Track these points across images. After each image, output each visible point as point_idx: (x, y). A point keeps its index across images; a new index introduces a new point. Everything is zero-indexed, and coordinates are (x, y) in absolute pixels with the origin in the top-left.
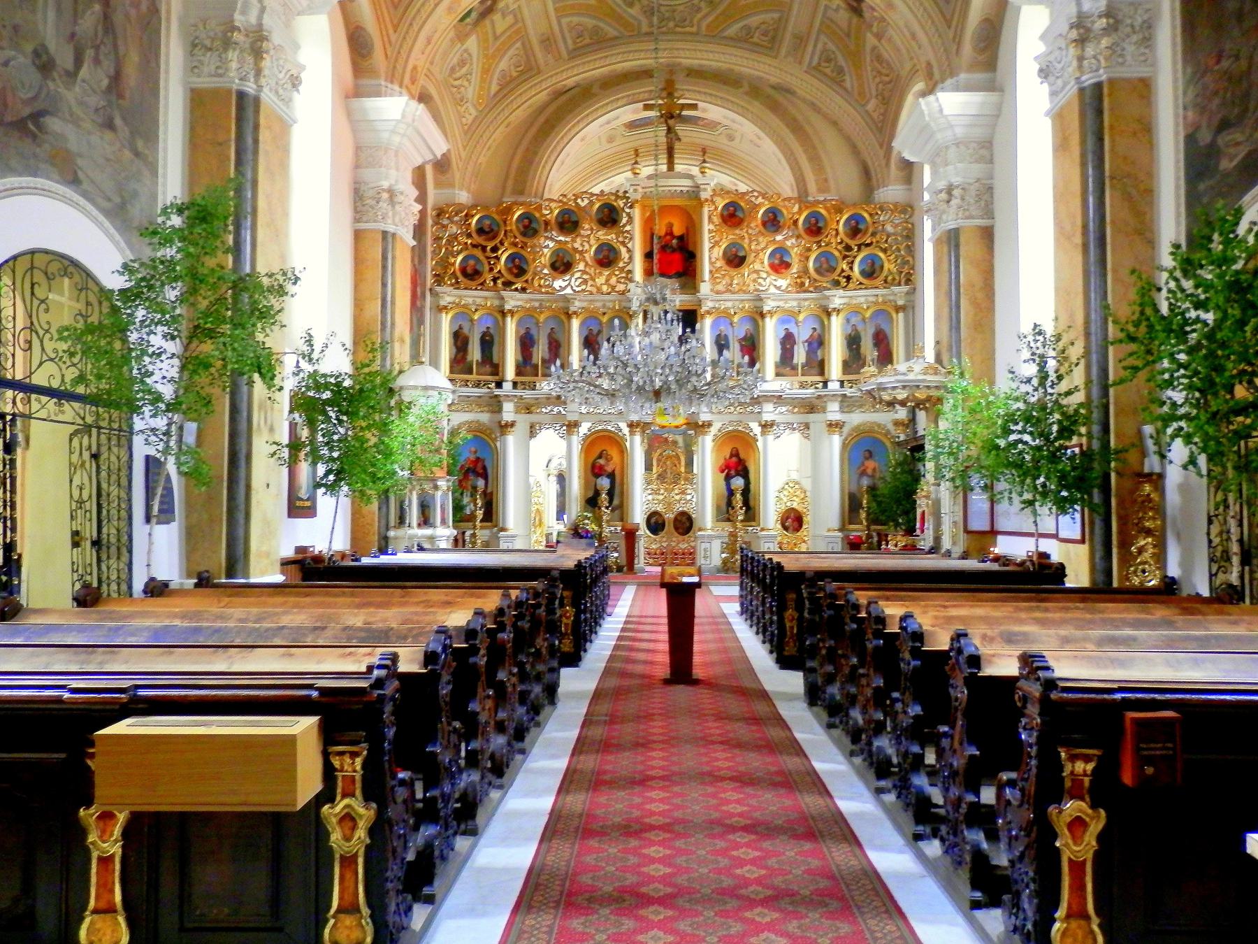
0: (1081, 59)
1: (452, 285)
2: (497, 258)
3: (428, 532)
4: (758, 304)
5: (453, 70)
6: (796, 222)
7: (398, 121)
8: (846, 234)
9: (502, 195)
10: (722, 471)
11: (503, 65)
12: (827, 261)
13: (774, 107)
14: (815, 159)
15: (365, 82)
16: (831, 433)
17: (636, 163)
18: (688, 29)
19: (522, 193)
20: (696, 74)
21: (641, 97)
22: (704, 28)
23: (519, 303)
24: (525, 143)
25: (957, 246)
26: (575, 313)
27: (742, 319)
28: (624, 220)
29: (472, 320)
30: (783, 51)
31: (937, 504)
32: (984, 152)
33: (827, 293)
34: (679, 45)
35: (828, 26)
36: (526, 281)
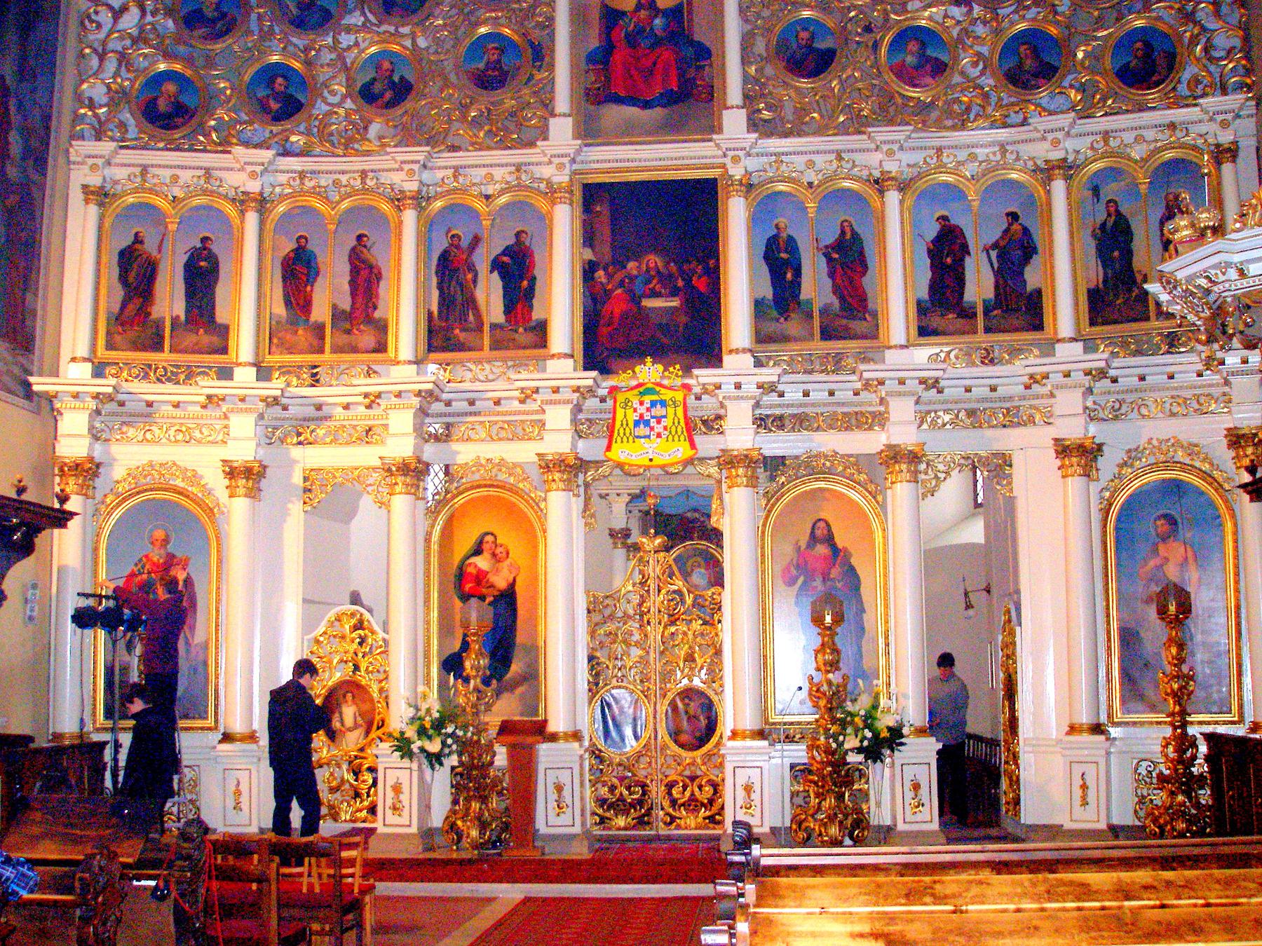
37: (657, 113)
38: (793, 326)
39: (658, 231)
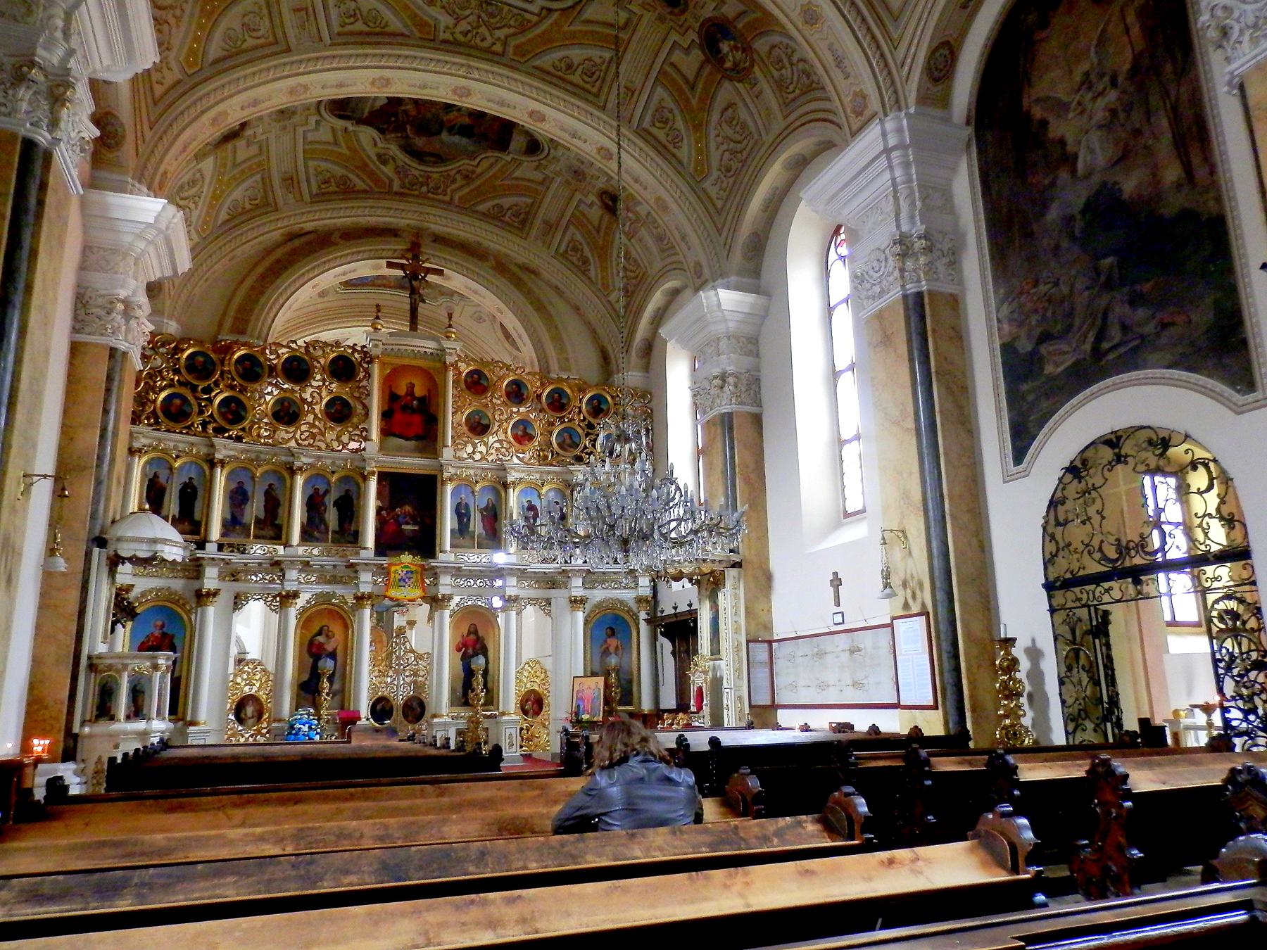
0: (902, 270)
1: (150, 425)
2: (210, 401)
3: (140, 725)
4: (501, 474)
5: (182, 187)
6: (539, 397)
7: (148, 225)
8: (588, 412)
9: (218, 332)
10: (459, 650)
11: (238, 194)
12: (571, 437)
13: (518, 283)
14: (557, 339)
15: (103, 174)
16: (573, 609)
17: (378, 318)
18: (441, 197)
19: (243, 332)
20: (439, 240)
21: (384, 254)
22: (456, 198)
23: (232, 453)
24: (249, 282)
25: (731, 429)
26: (300, 469)
27: (483, 489)
28: (362, 375)
29: (171, 469)
30: (534, 232)
31: (717, 683)
32: (750, 347)
33: (571, 468)
34: (428, 210)
35: (578, 221)
36: (243, 429)
37: (412, 444)
38: (466, 542)
39: (413, 499)
